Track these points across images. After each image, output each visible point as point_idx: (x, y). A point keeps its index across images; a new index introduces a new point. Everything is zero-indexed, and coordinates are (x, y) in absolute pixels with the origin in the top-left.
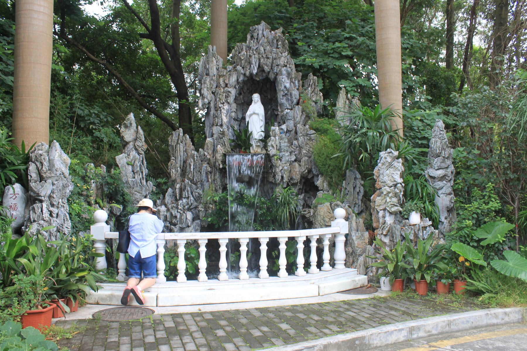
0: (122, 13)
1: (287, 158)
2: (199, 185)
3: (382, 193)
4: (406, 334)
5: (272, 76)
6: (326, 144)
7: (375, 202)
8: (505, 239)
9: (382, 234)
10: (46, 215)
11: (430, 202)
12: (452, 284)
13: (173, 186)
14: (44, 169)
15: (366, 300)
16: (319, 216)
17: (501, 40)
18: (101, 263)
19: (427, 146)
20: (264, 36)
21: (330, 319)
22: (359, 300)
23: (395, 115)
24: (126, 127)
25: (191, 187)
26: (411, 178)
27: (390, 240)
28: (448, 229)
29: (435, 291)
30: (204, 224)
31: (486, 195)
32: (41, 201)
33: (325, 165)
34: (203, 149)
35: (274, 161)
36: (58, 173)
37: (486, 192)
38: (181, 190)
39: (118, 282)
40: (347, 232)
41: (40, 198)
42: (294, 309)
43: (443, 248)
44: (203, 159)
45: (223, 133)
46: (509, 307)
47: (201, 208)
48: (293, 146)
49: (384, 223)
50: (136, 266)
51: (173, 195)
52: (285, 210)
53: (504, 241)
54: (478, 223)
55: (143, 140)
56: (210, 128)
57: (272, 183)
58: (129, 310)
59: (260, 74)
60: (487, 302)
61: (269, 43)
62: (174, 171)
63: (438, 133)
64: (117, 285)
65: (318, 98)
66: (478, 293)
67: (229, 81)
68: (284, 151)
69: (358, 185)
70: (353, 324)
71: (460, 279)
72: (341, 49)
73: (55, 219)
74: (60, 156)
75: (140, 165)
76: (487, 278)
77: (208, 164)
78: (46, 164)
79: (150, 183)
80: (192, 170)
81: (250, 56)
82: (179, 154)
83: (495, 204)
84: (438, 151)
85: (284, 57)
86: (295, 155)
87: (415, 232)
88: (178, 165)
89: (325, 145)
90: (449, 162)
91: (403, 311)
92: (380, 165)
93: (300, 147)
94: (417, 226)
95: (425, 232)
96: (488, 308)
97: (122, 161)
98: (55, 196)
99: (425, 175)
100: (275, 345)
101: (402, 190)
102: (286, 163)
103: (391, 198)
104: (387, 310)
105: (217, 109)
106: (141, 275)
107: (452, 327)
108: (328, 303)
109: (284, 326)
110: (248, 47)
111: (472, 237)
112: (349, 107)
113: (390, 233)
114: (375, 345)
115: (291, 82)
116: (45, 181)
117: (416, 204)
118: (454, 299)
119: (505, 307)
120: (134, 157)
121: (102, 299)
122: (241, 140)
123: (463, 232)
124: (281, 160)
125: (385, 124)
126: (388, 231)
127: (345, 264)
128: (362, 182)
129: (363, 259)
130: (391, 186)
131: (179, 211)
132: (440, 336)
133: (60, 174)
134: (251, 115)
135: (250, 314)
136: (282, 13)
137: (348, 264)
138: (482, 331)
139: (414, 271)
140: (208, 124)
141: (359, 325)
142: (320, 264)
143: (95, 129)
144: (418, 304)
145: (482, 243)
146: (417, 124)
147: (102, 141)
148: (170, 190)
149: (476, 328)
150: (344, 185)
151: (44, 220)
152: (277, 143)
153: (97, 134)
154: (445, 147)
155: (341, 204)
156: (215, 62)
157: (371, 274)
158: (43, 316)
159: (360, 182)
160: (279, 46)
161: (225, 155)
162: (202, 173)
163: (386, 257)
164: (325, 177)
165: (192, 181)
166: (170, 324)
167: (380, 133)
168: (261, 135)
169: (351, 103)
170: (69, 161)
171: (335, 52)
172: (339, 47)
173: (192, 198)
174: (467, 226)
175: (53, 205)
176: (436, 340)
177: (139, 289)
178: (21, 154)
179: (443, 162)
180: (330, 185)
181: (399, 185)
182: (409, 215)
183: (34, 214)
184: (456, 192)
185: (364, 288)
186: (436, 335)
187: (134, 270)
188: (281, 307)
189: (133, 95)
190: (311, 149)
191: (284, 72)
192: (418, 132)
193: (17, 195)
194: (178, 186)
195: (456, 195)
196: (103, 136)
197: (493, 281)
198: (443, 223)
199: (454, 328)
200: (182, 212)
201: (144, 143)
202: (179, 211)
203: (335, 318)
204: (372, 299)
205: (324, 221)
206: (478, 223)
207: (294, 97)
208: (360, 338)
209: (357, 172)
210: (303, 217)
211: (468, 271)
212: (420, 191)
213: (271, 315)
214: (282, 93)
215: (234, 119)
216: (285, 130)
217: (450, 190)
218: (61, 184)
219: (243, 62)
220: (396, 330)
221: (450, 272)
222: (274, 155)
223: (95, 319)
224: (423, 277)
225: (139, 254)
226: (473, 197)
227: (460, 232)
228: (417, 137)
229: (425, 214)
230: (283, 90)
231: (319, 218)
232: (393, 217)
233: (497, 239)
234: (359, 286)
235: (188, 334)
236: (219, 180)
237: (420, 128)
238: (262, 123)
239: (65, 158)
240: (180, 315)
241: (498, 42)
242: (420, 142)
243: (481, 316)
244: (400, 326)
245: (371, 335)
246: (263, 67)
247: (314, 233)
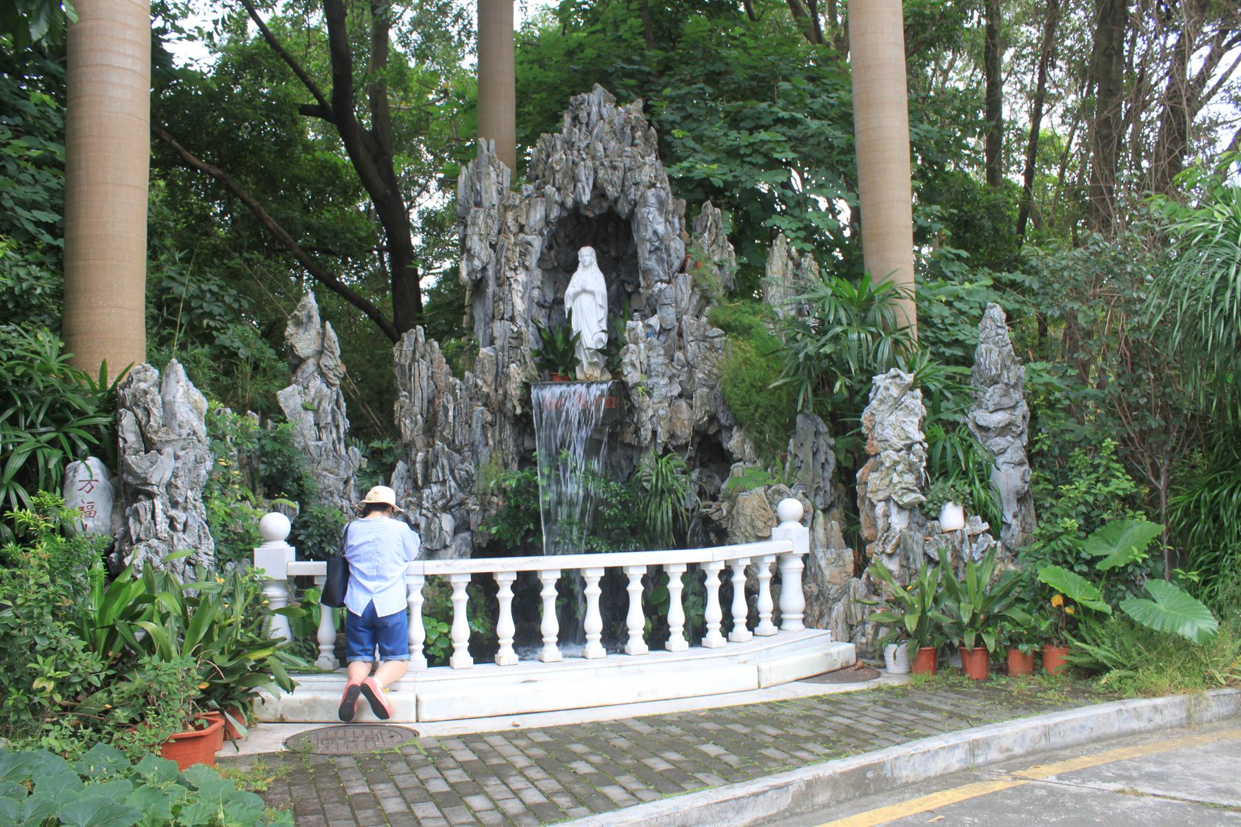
0: (260, 59)
1: (664, 391)
2: (467, 454)
3: (882, 463)
4: (963, 756)
5: (623, 208)
6: (748, 359)
7: (866, 483)
8: (1146, 556)
9: (883, 552)
10: (162, 525)
11: (981, 481)
12: (1039, 656)
13: (407, 457)
14: (152, 423)
15: (862, 692)
16: (741, 518)
17: (1110, 127)
18: (279, 627)
19: (968, 361)
20: (602, 118)
21: (803, 733)
22: (848, 693)
23: (903, 294)
24: (299, 323)
25: (449, 458)
26: (940, 431)
27: (902, 566)
28: (1020, 540)
29: (1003, 670)
30: (480, 540)
31: (1099, 465)
32: (151, 496)
33: (747, 405)
34: (473, 371)
35: (637, 397)
36: (184, 432)
37: (1101, 458)
38: (427, 466)
39: (319, 672)
40: (807, 551)
41: (149, 488)
42: (715, 715)
43: (1017, 581)
44: (475, 395)
45: (519, 337)
46: (1160, 696)
47: (472, 504)
48: (674, 363)
49: (888, 528)
50: (365, 636)
51: (409, 477)
52: (664, 505)
53: (1144, 560)
54: (1090, 525)
55: (338, 352)
56: (487, 324)
57: (630, 445)
58: (358, 731)
59: (596, 202)
60: (1116, 686)
61: (619, 134)
62: (407, 422)
63: (994, 333)
64: (322, 678)
65: (726, 256)
66: (1095, 670)
67: (527, 218)
68: (657, 376)
69: (824, 448)
70: (853, 740)
71: (1055, 642)
72: (771, 145)
73: (181, 535)
74: (187, 393)
75: (333, 410)
76: (1113, 638)
77: (485, 405)
78: (157, 412)
79: (356, 452)
80: (451, 419)
81: (573, 162)
82: (417, 384)
83: (1123, 484)
84: (994, 372)
85: (650, 167)
86: (680, 383)
87: (954, 547)
88: (417, 409)
89: (746, 361)
90: (1017, 395)
91: (947, 711)
92: (874, 403)
93: (690, 366)
94: (958, 533)
95: (974, 546)
96: (1120, 698)
97: (291, 402)
98: (179, 483)
99: (965, 424)
100: (707, 785)
101: (925, 456)
102: (661, 402)
103: (901, 474)
104: (913, 711)
105: (501, 281)
106: (373, 655)
107: (1053, 739)
108: (785, 701)
109: (712, 749)
110: (567, 142)
111: (1078, 553)
112: (796, 276)
113: (902, 550)
114: (904, 781)
115: (667, 220)
116: (159, 451)
117: (953, 486)
118: (1045, 684)
119: (1154, 695)
120: (318, 391)
121: (293, 710)
122: (554, 352)
123: (1059, 543)
124: (650, 395)
125: (883, 317)
126: (898, 545)
127: (804, 620)
128: (832, 441)
129: (842, 609)
130: (901, 450)
131: (424, 512)
132: (1031, 759)
133: (189, 435)
134: (576, 295)
135: (629, 729)
136: (632, 62)
137: (810, 619)
138: (1113, 745)
139: (959, 627)
140: (482, 315)
141: (866, 741)
142: (753, 621)
143: (216, 329)
144: (974, 696)
145: (1099, 566)
146: (938, 311)
147: (235, 354)
148: (401, 466)
149: (1099, 739)
150: (791, 447)
151: (159, 539)
152: (643, 357)
153: (223, 339)
154: (1008, 363)
155: (787, 489)
156: (493, 175)
157: (864, 640)
158: (203, 743)
159: (827, 441)
160: (637, 141)
161: (526, 386)
162: (474, 426)
163: (897, 602)
164: (748, 430)
165: (450, 443)
166: (466, 756)
167: (872, 333)
168: (601, 340)
169: (798, 266)
170: (204, 404)
171: (755, 151)
172: (763, 142)
173: (453, 483)
174: (1067, 531)
175: (175, 504)
176: (1025, 766)
177: (378, 683)
178: (97, 392)
179: (1006, 394)
180: (759, 449)
181: (917, 446)
182: (939, 511)
183: (138, 525)
184: (1033, 457)
185: (849, 670)
186: (1021, 756)
187: (362, 644)
188: (688, 713)
189: (290, 247)
190: (715, 371)
191: (652, 200)
192: (942, 330)
193: (94, 483)
194: (420, 456)
195: (1031, 465)
196: (237, 344)
197: (1126, 645)
198: (1009, 526)
199: (1056, 740)
200: (429, 515)
201: (339, 362)
202: (424, 512)
203: (811, 730)
204: (874, 690)
205: (753, 527)
206: (1090, 525)
207: (674, 256)
208: (875, 765)
209: (820, 420)
210: (706, 520)
211: (1072, 624)
212: (961, 456)
213: (675, 730)
214: (648, 245)
215: (538, 304)
216: (658, 328)
217: (1021, 455)
218: (191, 455)
219: (557, 176)
220: (943, 748)
221: (1035, 628)
222: (637, 385)
223: (294, 751)
224: (979, 641)
225: (371, 609)
226: (1071, 469)
227: (1053, 544)
228: (942, 342)
229: (974, 508)
230: (649, 240)
231: (742, 522)
232: (906, 514)
233: (1131, 557)
234: (838, 666)
235: (514, 772)
236: (511, 442)
237: (947, 321)
238: (603, 313)
239: (196, 398)
240: (479, 737)
241: (1105, 132)
242: (948, 352)
243: (1108, 715)
244: (950, 739)
245: (896, 758)
246: (603, 189)
247: (741, 553)
